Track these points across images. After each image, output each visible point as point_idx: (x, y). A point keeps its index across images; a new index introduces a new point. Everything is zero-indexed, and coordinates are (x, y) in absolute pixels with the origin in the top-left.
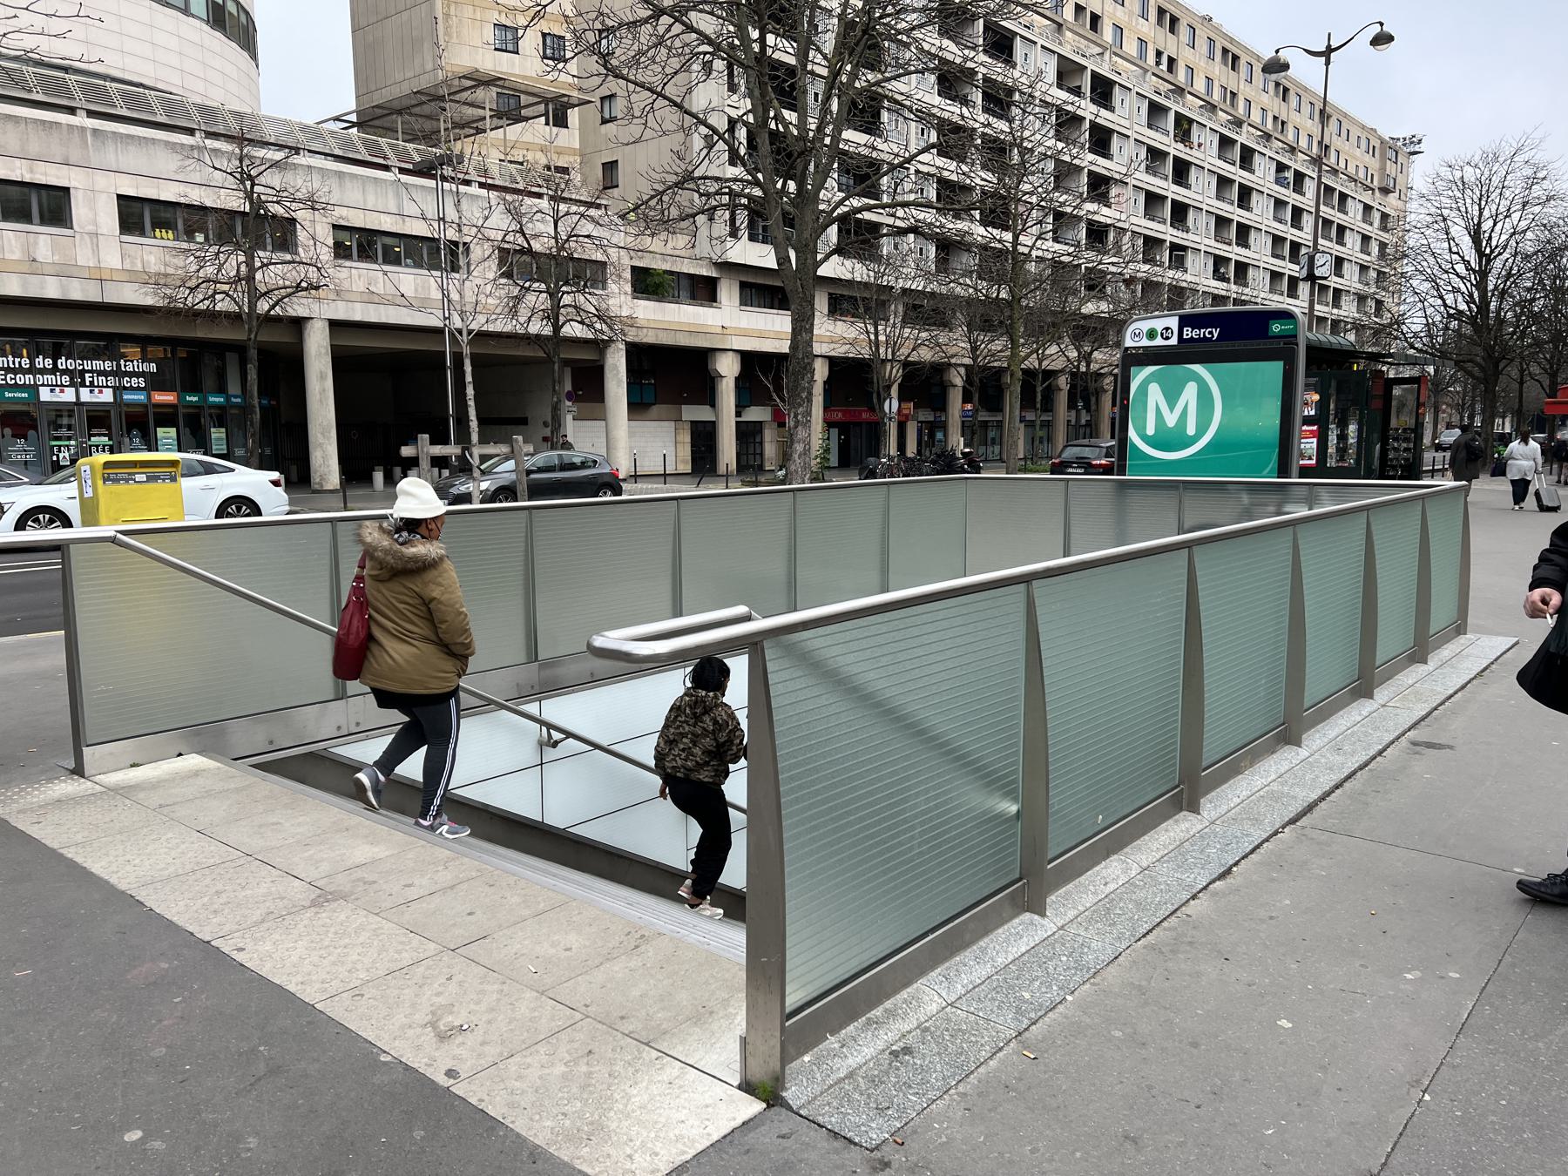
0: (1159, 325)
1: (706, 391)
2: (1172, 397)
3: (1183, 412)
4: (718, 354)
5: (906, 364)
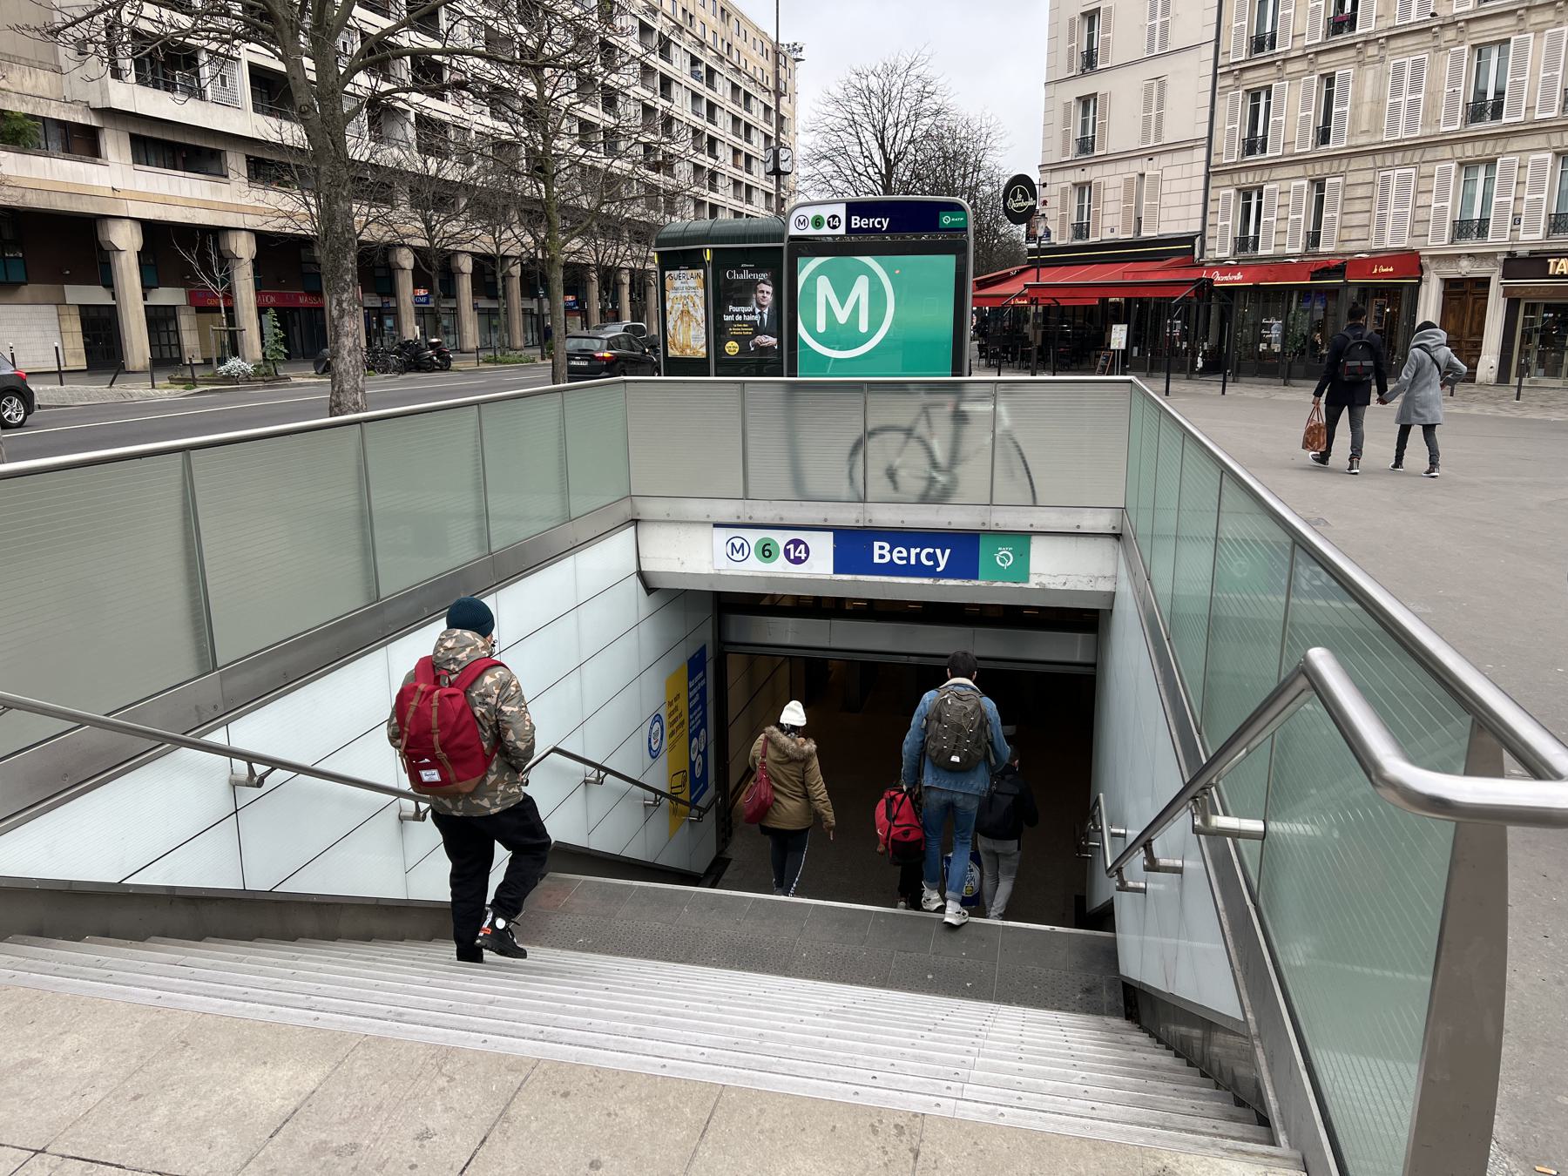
0: (825, 212)
1: (99, 266)
2: (842, 293)
3: (856, 309)
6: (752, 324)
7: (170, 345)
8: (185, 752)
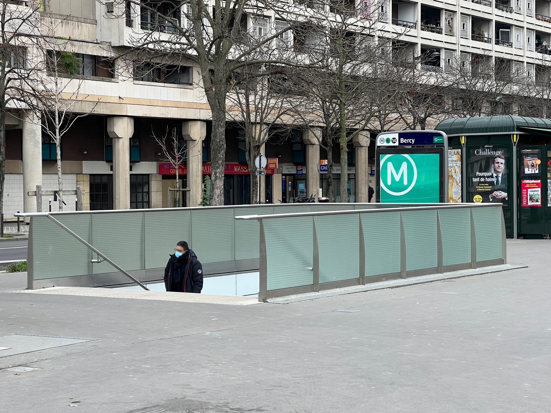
2: (397, 168)
4: (116, 120)
5: (273, 127)
6: (491, 183)
7: (143, 192)
8: (139, 286)
